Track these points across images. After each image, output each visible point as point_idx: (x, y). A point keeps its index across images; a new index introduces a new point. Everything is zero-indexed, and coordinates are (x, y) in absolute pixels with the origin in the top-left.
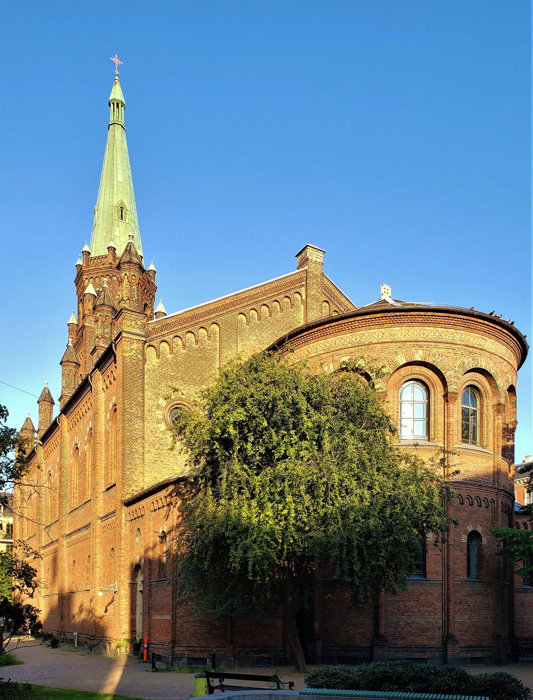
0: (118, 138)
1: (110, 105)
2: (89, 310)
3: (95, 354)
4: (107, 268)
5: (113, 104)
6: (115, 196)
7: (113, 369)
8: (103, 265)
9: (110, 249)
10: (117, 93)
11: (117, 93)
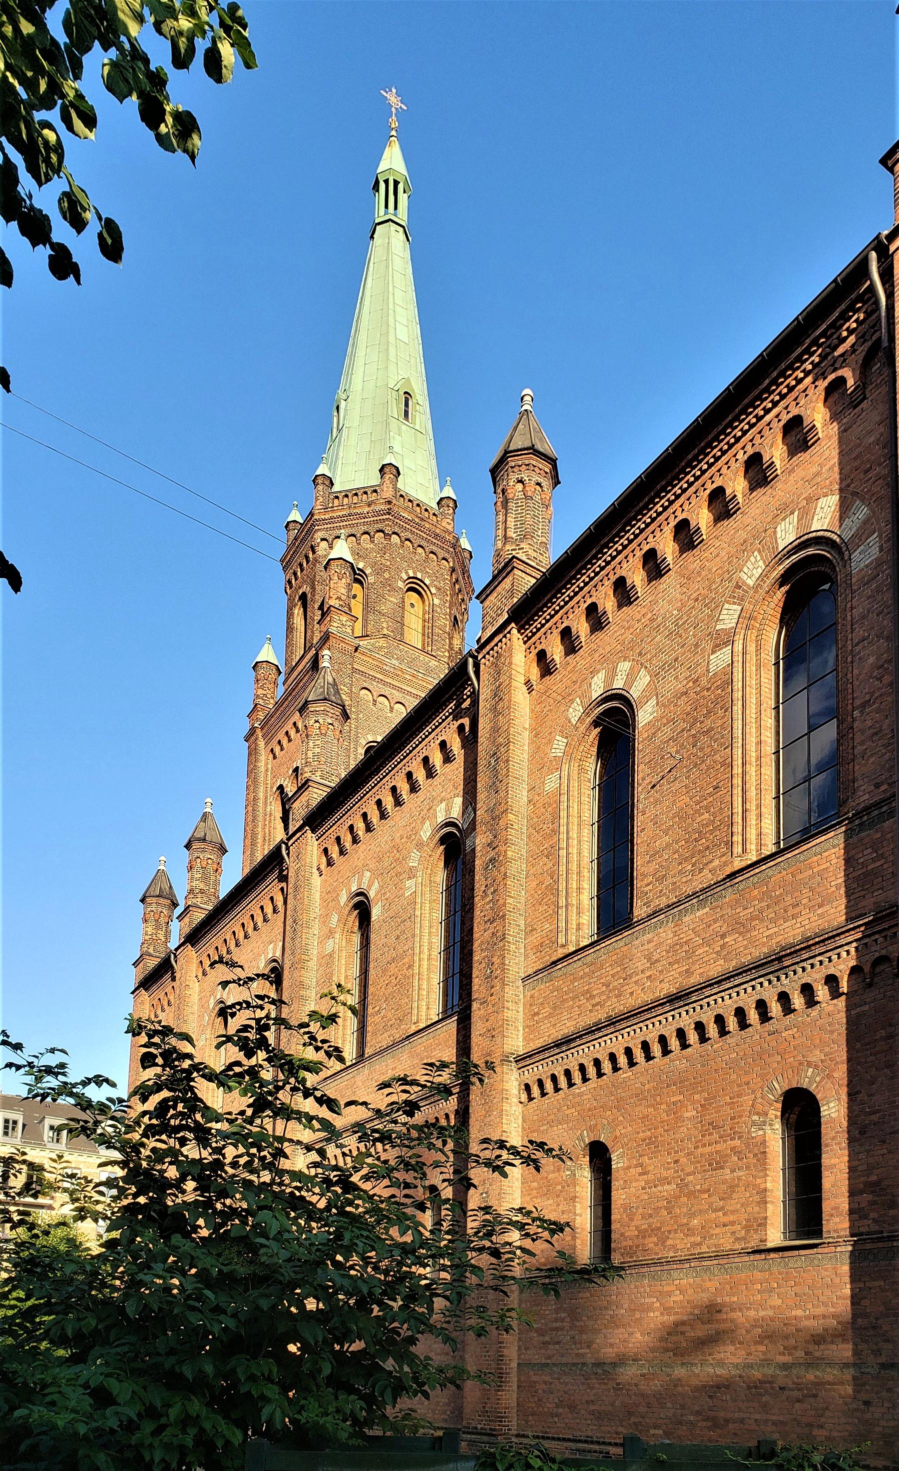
0: (391, 259)
1: (376, 187)
2: (339, 598)
3: (186, 920)
4: (378, 513)
5: (386, 182)
6: (392, 367)
7: (169, 989)
8: (369, 505)
9: (386, 470)
10: (393, 161)
11: (393, 161)
